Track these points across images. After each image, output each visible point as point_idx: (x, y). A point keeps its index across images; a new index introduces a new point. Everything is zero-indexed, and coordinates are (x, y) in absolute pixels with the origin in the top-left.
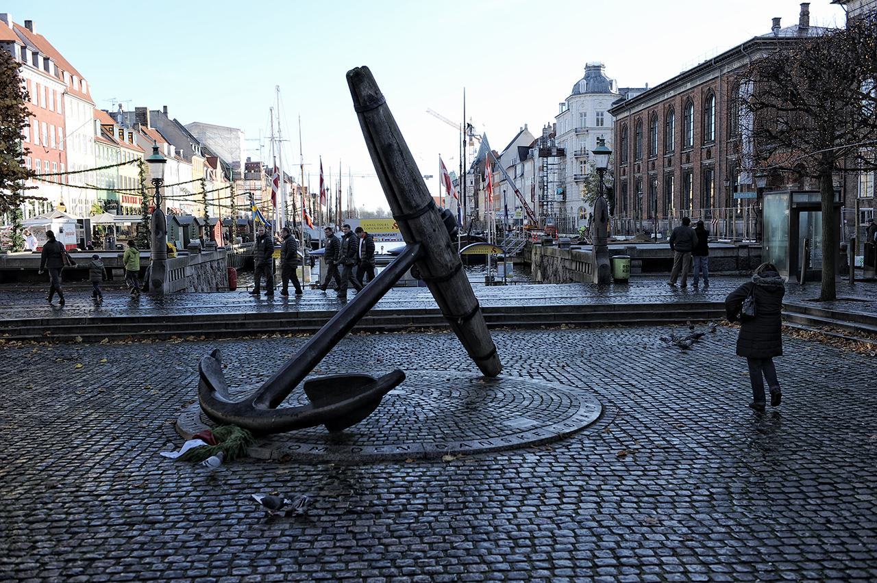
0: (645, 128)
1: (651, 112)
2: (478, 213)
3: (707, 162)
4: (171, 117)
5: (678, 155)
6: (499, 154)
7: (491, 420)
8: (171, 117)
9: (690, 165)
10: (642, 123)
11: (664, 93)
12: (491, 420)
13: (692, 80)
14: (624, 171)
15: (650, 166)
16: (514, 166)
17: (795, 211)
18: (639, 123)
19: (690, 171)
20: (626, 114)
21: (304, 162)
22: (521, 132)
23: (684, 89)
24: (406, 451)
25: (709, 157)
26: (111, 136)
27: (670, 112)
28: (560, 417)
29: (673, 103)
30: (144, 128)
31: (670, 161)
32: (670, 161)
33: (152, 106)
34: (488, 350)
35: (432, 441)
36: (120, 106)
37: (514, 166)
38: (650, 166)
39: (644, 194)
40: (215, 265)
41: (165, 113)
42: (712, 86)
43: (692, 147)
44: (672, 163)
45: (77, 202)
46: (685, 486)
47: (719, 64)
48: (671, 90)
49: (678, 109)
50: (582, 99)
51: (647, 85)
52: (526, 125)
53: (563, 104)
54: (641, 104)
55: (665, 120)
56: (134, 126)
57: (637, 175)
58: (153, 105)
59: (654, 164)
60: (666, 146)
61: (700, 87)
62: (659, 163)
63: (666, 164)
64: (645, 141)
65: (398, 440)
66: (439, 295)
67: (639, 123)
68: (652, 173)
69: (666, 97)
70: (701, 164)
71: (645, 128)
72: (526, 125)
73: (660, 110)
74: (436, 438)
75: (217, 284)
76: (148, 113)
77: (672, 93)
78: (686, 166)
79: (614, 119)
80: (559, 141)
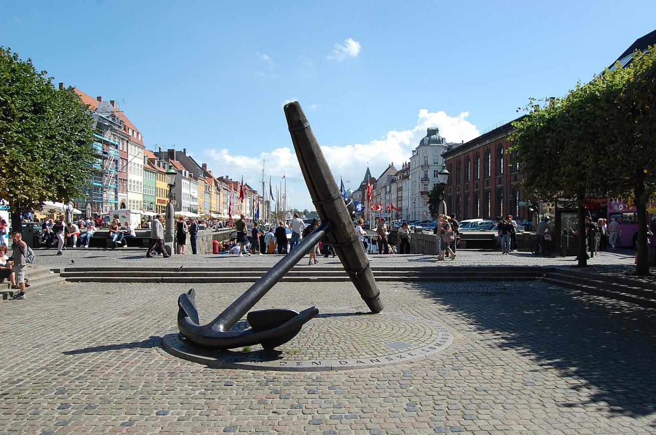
0: (462, 165)
1: (466, 156)
2: (363, 214)
3: (499, 186)
4: (187, 155)
5: (481, 181)
6: (376, 179)
7: (377, 343)
8: (187, 155)
9: (489, 187)
10: (461, 162)
11: (474, 146)
12: (377, 343)
13: (489, 138)
14: (450, 190)
15: (465, 188)
16: (385, 187)
17: (558, 212)
18: (459, 163)
19: (489, 191)
20: (451, 157)
21: (265, 181)
22: (390, 167)
23: (485, 144)
24: (318, 366)
25: (500, 183)
26: (153, 165)
27: (477, 156)
28: (425, 342)
29: (479, 151)
30: (172, 161)
31: (477, 185)
32: (477, 185)
33: (177, 149)
34: (375, 293)
35: (336, 358)
36: (160, 148)
37: (385, 187)
38: (465, 188)
39: (462, 205)
40: (205, 238)
41: (185, 152)
42: (502, 142)
43: (490, 177)
44: (489, 184)
45: (132, 202)
46: (478, 402)
47: (505, 130)
48: (478, 144)
49: (481, 155)
50: (425, 148)
51: (463, 141)
52: (392, 163)
53: (414, 151)
54: (460, 151)
55: (465, 164)
56: (167, 160)
57: (458, 193)
58: (178, 149)
59: (467, 186)
60: (466, 179)
61: (494, 143)
62: (471, 186)
63: (475, 187)
64: (462, 173)
65: (313, 357)
66: (344, 260)
67: (459, 163)
68: (466, 191)
69: (474, 148)
70: (496, 187)
71: (462, 165)
72: (392, 163)
73: (471, 155)
74: (340, 356)
75: (205, 251)
76: (175, 153)
77: (478, 146)
78: (486, 188)
79: (444, 160)
80: (412, 172)
